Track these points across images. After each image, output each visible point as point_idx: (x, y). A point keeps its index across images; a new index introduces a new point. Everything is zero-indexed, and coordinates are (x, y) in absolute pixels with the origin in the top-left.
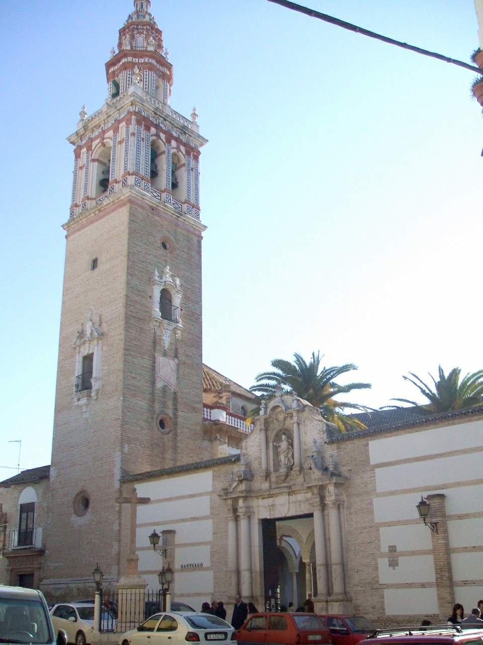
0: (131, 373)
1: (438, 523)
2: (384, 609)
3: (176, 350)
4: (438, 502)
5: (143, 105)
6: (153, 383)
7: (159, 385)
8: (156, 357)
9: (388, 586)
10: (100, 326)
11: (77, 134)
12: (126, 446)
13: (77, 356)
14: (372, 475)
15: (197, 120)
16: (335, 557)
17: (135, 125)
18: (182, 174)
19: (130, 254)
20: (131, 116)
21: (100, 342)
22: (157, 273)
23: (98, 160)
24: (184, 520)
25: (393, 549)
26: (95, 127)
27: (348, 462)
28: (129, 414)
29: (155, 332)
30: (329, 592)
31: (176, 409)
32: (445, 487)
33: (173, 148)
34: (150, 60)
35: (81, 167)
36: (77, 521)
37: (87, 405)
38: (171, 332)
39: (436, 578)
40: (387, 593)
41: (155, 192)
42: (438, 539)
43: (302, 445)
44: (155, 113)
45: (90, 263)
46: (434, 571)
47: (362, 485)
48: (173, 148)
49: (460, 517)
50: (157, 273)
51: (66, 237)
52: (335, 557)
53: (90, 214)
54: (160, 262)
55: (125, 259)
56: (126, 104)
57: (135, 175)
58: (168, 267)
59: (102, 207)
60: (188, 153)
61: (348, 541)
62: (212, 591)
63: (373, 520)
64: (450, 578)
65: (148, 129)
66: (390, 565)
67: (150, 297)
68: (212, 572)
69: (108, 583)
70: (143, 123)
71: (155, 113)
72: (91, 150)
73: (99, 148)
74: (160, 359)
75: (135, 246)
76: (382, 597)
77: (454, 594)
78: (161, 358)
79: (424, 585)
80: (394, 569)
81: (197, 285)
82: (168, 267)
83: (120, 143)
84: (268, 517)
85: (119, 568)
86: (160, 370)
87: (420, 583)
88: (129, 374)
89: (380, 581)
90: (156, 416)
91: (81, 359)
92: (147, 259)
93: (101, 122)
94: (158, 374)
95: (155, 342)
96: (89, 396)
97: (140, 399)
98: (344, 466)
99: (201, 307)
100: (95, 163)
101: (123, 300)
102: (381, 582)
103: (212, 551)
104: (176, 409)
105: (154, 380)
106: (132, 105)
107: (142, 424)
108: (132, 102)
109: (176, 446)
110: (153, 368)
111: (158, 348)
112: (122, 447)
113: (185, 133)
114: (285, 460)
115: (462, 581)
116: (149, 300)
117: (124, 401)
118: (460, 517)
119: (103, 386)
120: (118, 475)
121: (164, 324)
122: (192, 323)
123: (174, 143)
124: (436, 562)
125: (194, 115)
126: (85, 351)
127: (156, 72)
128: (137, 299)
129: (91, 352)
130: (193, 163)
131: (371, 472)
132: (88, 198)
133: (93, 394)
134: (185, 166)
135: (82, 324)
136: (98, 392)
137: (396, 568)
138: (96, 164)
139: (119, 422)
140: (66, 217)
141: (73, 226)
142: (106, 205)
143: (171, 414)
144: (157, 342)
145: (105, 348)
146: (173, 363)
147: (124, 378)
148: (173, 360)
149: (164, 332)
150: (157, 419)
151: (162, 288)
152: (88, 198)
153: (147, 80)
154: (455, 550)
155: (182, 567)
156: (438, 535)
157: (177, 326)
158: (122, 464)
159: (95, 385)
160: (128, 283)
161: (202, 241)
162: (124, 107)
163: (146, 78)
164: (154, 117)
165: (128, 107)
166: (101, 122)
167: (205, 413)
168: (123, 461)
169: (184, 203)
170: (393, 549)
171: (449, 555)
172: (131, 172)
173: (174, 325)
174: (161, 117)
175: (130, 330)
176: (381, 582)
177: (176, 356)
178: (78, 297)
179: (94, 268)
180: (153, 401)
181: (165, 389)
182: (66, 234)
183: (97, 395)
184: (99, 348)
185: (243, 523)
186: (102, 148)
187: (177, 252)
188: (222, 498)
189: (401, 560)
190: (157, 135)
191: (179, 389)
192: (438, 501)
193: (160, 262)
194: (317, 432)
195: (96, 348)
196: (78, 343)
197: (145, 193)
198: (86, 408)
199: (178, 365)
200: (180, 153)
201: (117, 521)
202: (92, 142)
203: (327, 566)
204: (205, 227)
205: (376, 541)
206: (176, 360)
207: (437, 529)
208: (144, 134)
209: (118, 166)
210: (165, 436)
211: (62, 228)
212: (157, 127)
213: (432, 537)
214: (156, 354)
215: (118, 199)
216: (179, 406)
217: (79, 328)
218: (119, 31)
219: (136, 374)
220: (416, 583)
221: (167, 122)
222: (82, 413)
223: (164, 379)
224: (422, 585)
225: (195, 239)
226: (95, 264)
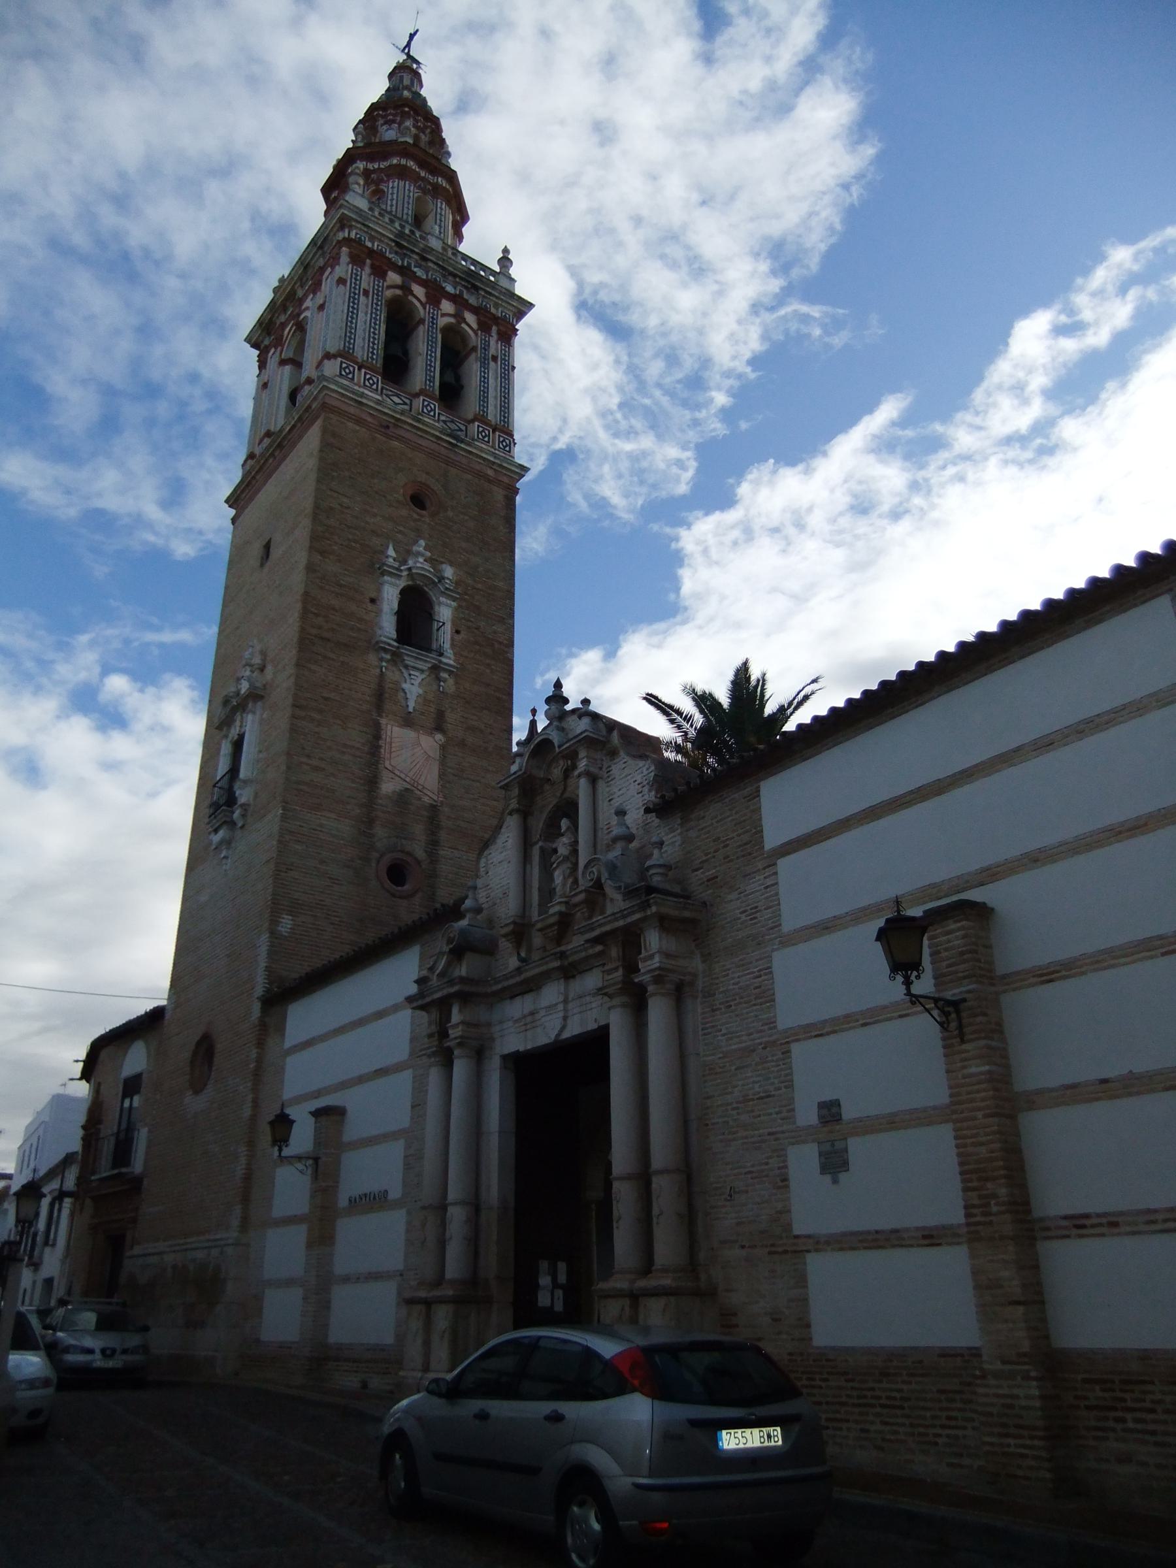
0: (308, 756)
1: (964, 1000)
2: (808, 1326)
3: (440, 715)
4: (959, 929)
5: (368, 227)
6: (372, 782)
7: (388, 787)
8: (383, 727)
9: (818, 1243)
14: (769, 882)
15: (513, 272)
16: (662, 1153)
17: (348, 264)
18: (472, 369)
22: (391, 552)
24: (361, 1080)
25: (830, 1111)
27: (706, 855)
29: (382, 674)
30: (647, 1267)
32: (989, 875)
33: (443, 315)
34: (403, 162)
36: (194, 1104)
38: (423, 676)
39: (966, 1207)
40: (818, 1265)
41: (398, 396)
42: (966, 1060)
43: (600, 834)
44: (398, 244)
46: (959, 1177)
47: (743, 917)
48: (443, 315)
49: (1048, 975)
50: (391, 552)
52: (662, 1153)
54: (400, 532)
57: (341, 356)
58: (422, 543)
60: (484, 327)
61: (708, 1098)
62: (401, 1267)
63: (771, 1023)
64: (1021, 1205)
65: (379, 272)
66: (824, 1169)
67: (373, 601)
68: (403, 1211)
70: (368, 261)
71: (398, 244)
73: (293, 335)
74: (395, 734)
75: (335, 495)
76: (802, 1280)
77: (1036, 1267)
78: (396, 729)
79: (931, 1237)
80: (835, 1181)
81: (501, 584)
82: (422, 543)
84: (521, 1049)
86: (393, 755)
87: (917, 1229)
88: (304, 760)
89: (795, 1226)
90: (375, 855)
92: (367, 523)
97: (333, 816)
98: (697, 870)
102: (798, 1229)
105: (375, 777)
112: (274, 922)
113: (477, 288)
114: (564, 884)
115: (1066, 1218)
116: (370, 606)
118: (1048, 975)
121: (406, 658)
122: (488, 661)
123: (447, 306)
124: (965, 1146)
125: (505, 261)
127: (416, 182)
130: (495, 346)
131: (768, 872)
134: (476, 351)
137: (843, 1177)
143: (420, 853)
144: (387, 695)
146: (430, 743)
147: (289, 768)
148: (431, 734)
149: (406, 675)
150: (378, 862)
151: (402, 583)
153: (395, 197)
154: (1035, 1100)
155: (350, 1201)
156: (964, 1047)
157: (440, 662)
159: (241, 794)
160: (310, 568)
162: (330, 238)
163: (392, 194)
164: (396, 253)
169: (473, 421)
170: (830, 1111)
171: (1013, 1117)
172: (332, 351)
173: (432, 658)
174: (413, 252)
175: (313, 667)
176: (798, 1229)
177: (439, 728)
180: (371, 822)
181: (403, 798)
183: (243, 816)
185: (461, 1068)
187: (450, 514)
188: (415, 1004)
189: (857, 1148)
190: (406, 289)
191: (445, 797)
192: (959, 925)
193: (400, 532)
194: (634, 788)
197: (366, 392)
199: (443, 748)
200: (464, 325)
201: (250, 1097)
203: (643, 1177)
205: (784, 1090)
206: (439, 737)
207: (960, 1027)
208: (366, 279)
211: (227, 505)
212: (403, 271)
213: (946, 1055)
214: (383, 721)
216: (443, 835)
219: (321, 759)
220: (907, 1230)
223: (403, 776)
224: (924, 1237)
225: (499, 494)
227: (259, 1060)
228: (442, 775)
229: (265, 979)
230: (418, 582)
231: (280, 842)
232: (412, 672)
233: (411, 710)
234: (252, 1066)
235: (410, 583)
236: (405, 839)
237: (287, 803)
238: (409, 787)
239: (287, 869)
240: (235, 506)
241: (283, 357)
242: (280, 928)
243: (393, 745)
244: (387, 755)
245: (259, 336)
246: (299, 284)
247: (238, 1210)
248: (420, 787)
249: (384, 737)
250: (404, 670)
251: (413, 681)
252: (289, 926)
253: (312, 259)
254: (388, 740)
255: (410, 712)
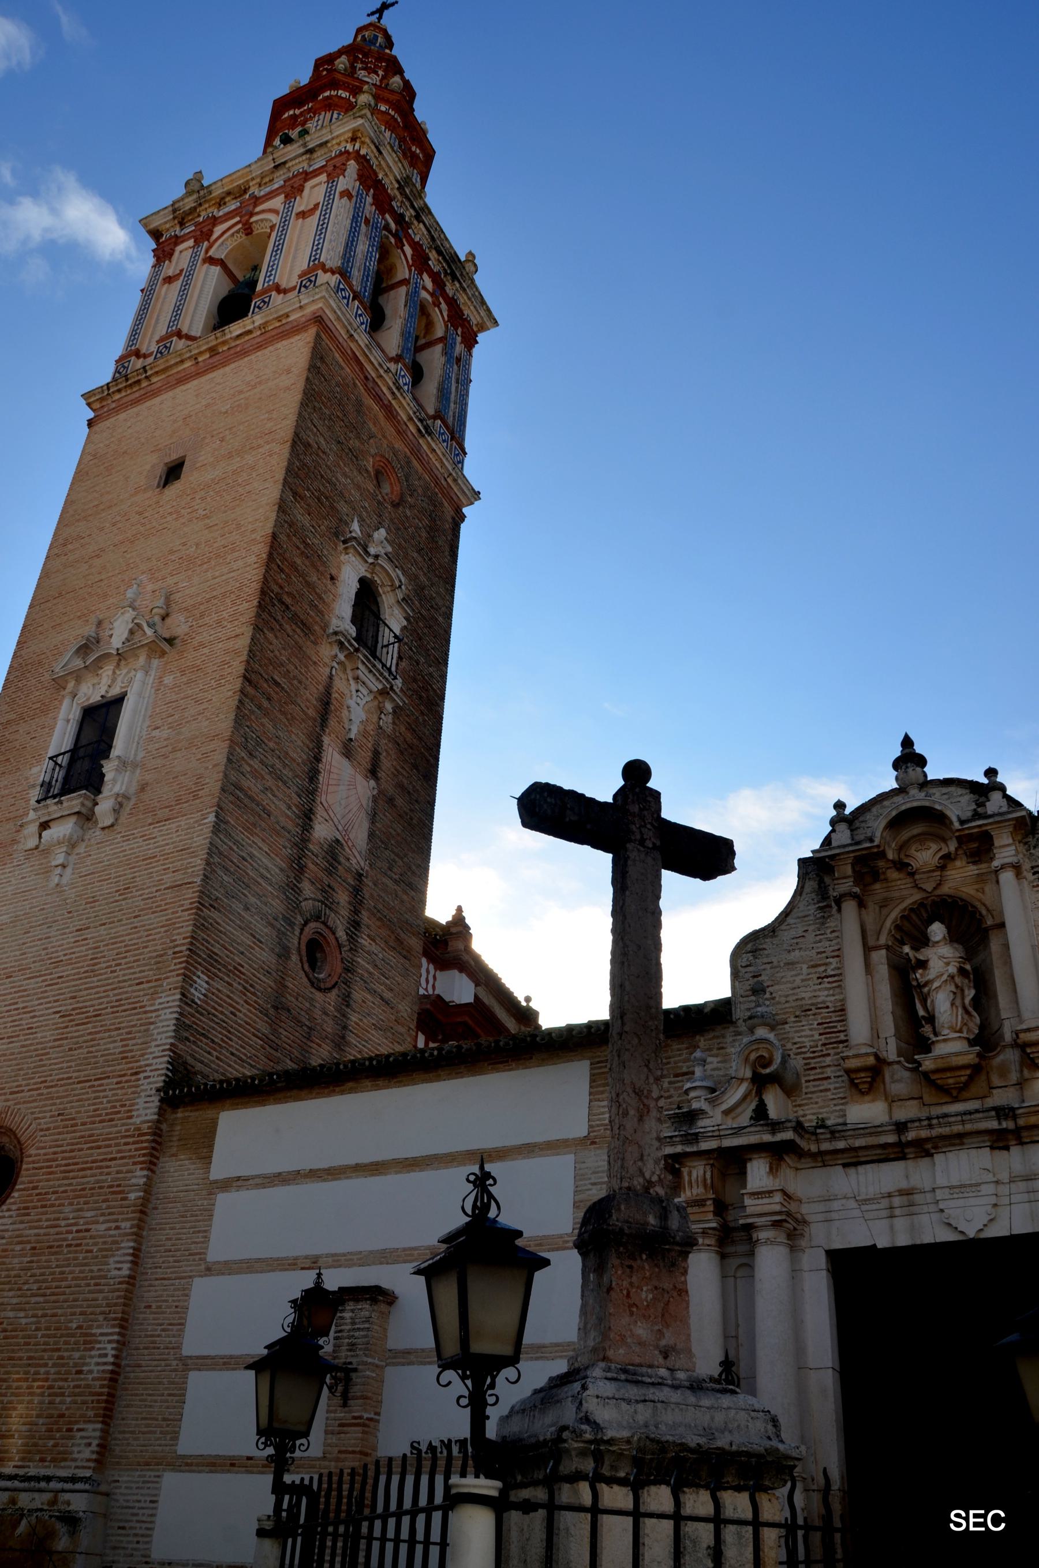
6: (307, 816)
7: (322, 831)
10: (163, 619)
11: (174, 208)
12: (201, 982)
13: (66, 702)
19: (298, 443)
20: (348, 160)
21: (155, 662)
23: (221, 263)
26: (229, 193)
28: (225, 878)
31: (355, 924)
35: (170, 277)
37: (72, 844)
45: (160, 470)
51: (90, 423)
53: (182, 361)
55: (285, 450)
56: (337, 136)
59: (224, 343)
69: (47, 1496)
72: (208, 240)
74: (332, 757)
83: (303, 215)
85: (105, 1433)
91: (76, 714)
93: (253, 179)
94: (324, 797)
95: (326, 706)
96: (86, 817)
99: (443, 677)
100: (213, 267)
101: (261, 550)
103: (577, 1198)
104: (355, 924)
106: (354, 139)
107: (263, 930)
108: (355, 131)
109: (343, 1037)
110: (313, 775)
111: (332, 722)
117: (216, 829)
119: (143, 788)
120: (154, 1074)
126: (93, 692)
128: (298, 561)
129: (115, 691)
132: (179, 334)
133: (104, 806)
135: (100, 623)
136: (121, 805)
138: (216, 270)
139: (190, 895)
140: (105, 375)
141: (117, 396)
142: (238, 336)
145: (168, 680)
150: (302, 930)
152: (179, 334)
158: (178, 1037)
159: (114, 780)
161: (462, 525)
165: (339, 144)
166: (253, 179)
167: (423, 971)
168: (183, 1027)
178: (98, 556)
179: (164, 486)
181: (334, 850)
182: (91, 415)
183: (117, 811)
184: (151, 680)
186: (241, 238)
195: (140, 675)
196: (78, 663)
198: (68, 854)
201: (128, 1245)
202: (214, 225)
204: (477, 495)
209: (297, 232)
210: (319, 996)
214: (326, 740)
215: (279, 319)
216: (365, 916)
217: (89, 630)
218: (316, 61)
221: (421, 225)
222: (47, 871)
226: (173, 472)
227: (148, 1188)
228: (371, 835)
229: (169, 1063)
230: (376, 578)
231: (208, 864)
232: (361, 688)
233: (353, 736)
234: (132, 1196)
235: (369, 576)
236: (330, 908)
237: (221, 809)
238: (340, 839)
239: (211, 905)
240: (97, 406)
241: (210, 253)
242: (192, 990)
243: (332, 776)
244: (325, 788)
245: (166, 223)
246: (258, 180)
247: (93, 1430)
248: (350, 844)
249: (324, 760)
250: (352, 682)
251: (359, 701)
252: (204, 991)
253: (291, 160)
254: (328, 767)
255: (351, 740)
